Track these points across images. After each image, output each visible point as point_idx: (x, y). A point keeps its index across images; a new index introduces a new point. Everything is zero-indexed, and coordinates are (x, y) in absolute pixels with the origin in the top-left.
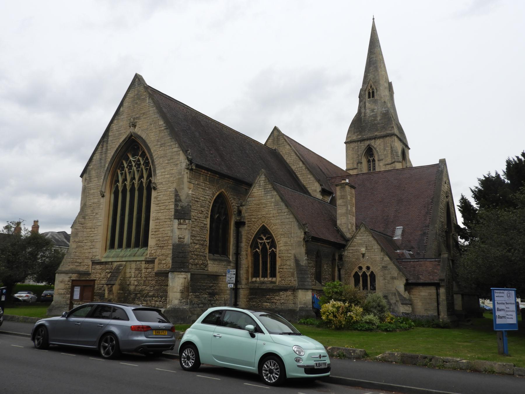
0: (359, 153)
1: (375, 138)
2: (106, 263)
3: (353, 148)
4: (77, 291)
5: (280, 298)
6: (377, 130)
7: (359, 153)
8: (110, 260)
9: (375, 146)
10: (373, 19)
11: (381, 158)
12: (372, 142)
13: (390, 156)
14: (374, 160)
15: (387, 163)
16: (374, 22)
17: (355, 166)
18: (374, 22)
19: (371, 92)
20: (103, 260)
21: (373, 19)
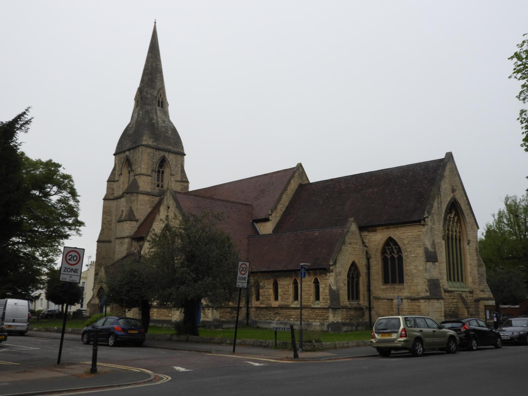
0: (154, 161)
1: (169, 151)
2: (451, 292)
3: (149, 154)
4: (488, 312)
5: (460, 305)
6: (170, 144)
7: (154, 161)
8: (453, 289)
9: (169, 160)
10: (155, 23)
11: (172, 173)
12: (166, 154)
13: (180, 174)
14: (163, 172)
15: (177, 179)
16: (155, 26)
17: (149, 173)
18: (155, 26)
19: (161, 101)
20: (450, 289)
21: (155, 23)
